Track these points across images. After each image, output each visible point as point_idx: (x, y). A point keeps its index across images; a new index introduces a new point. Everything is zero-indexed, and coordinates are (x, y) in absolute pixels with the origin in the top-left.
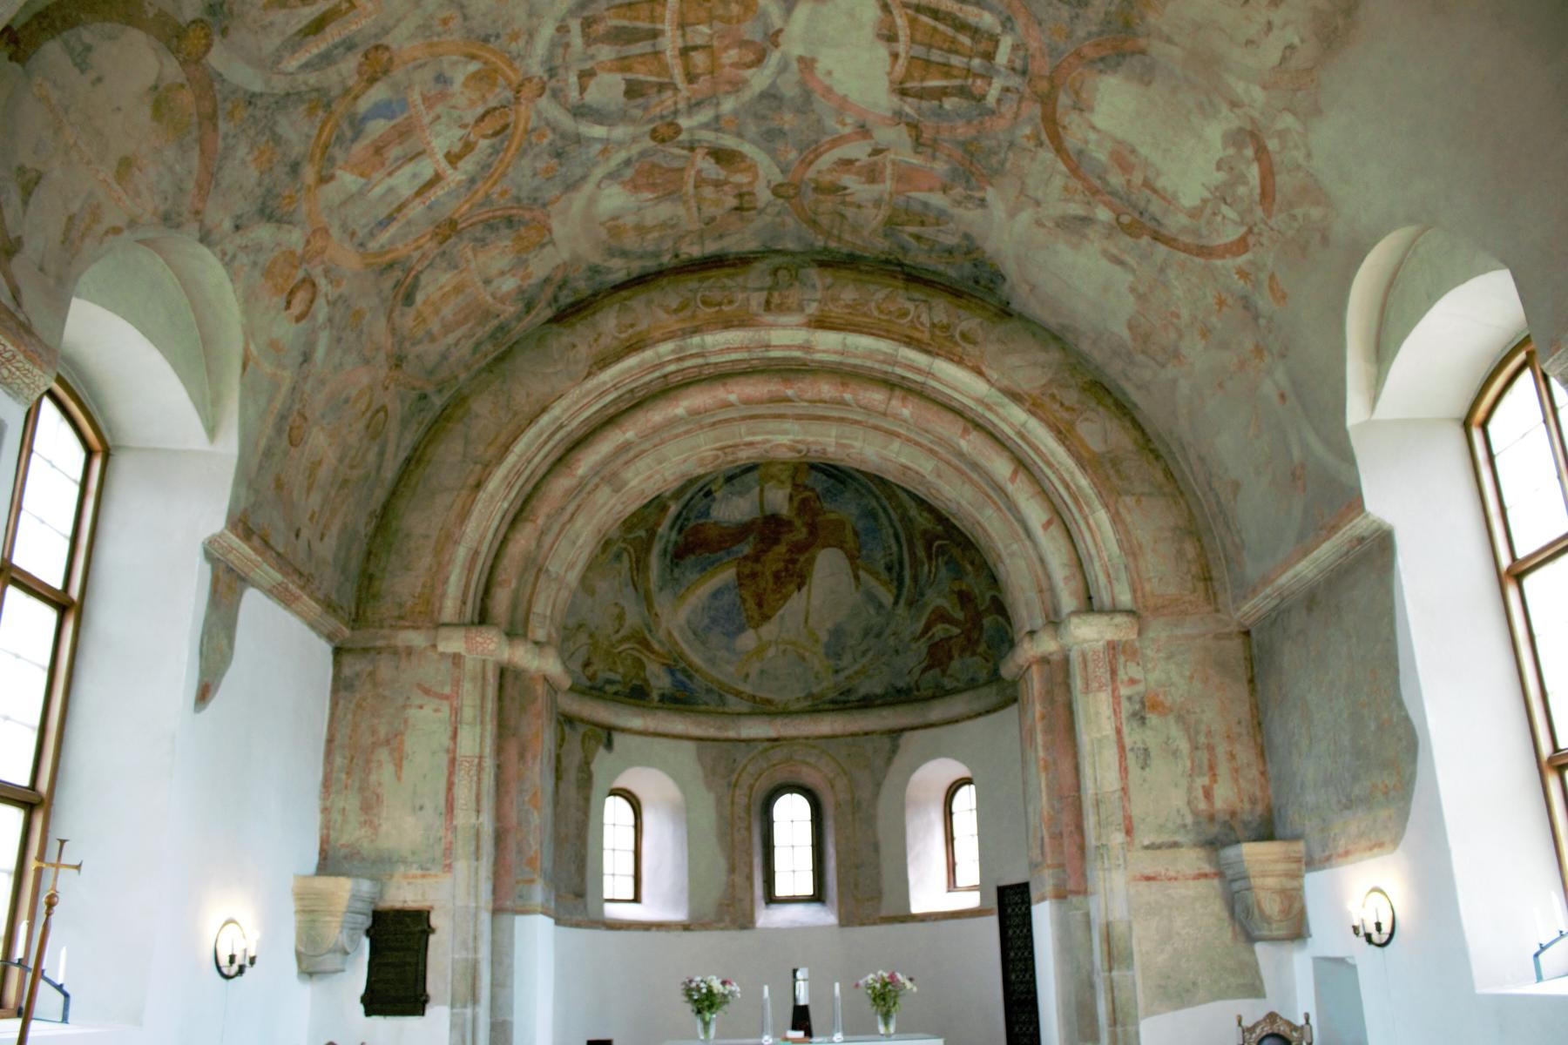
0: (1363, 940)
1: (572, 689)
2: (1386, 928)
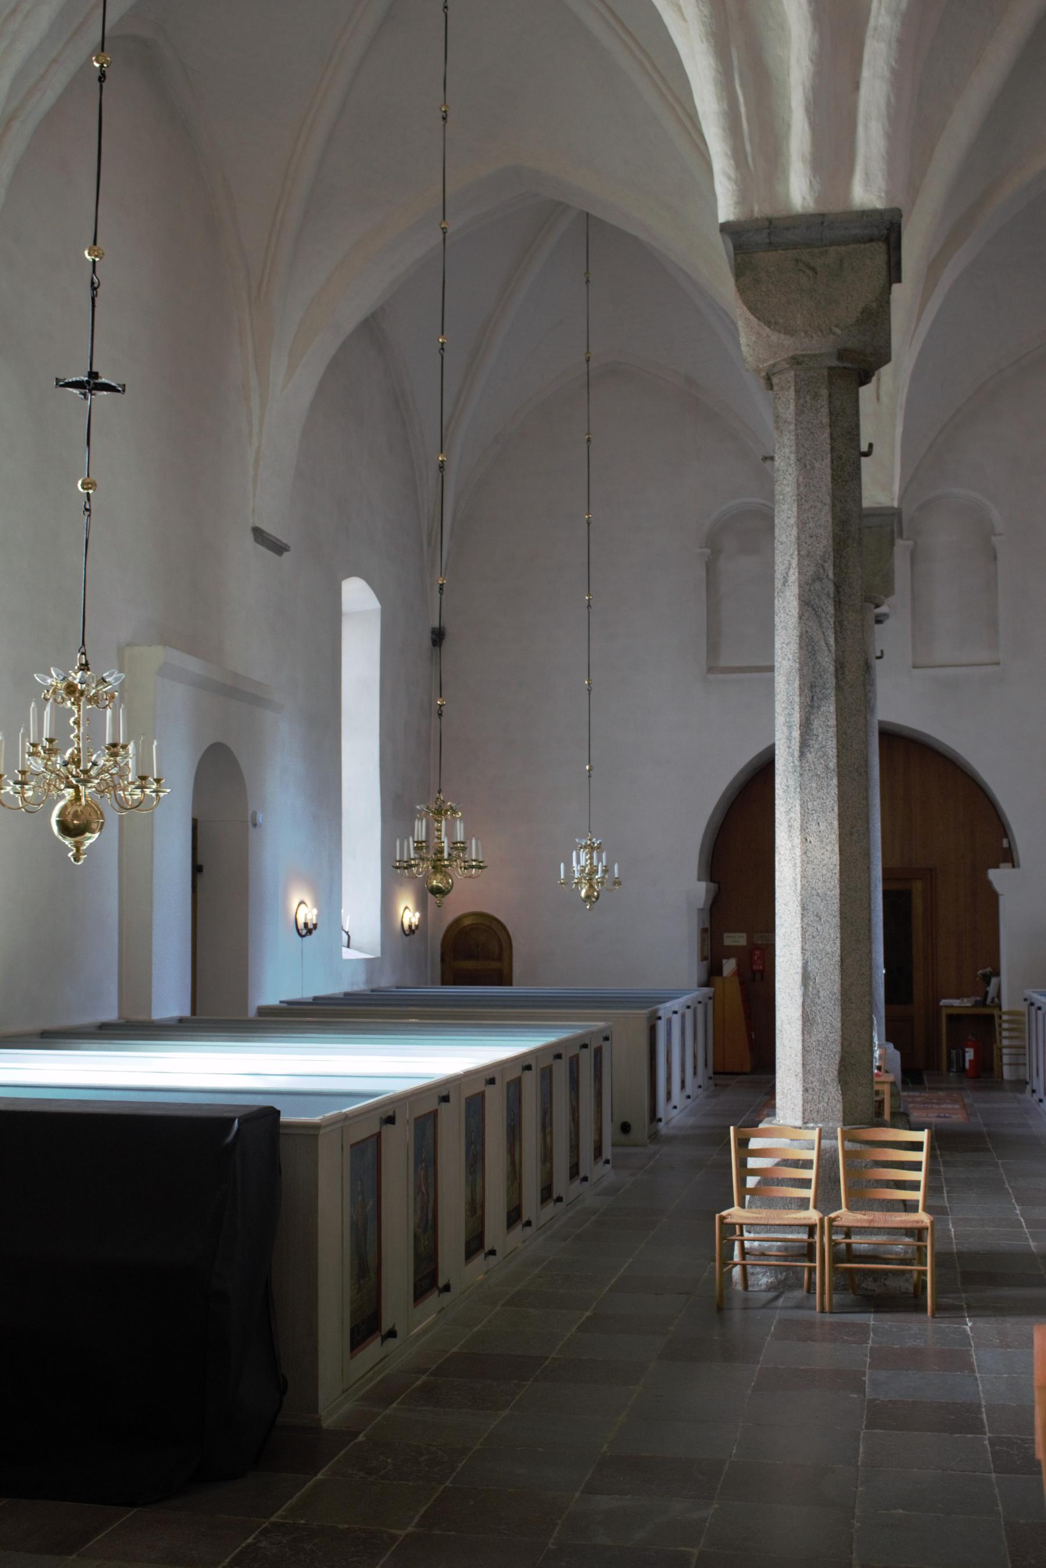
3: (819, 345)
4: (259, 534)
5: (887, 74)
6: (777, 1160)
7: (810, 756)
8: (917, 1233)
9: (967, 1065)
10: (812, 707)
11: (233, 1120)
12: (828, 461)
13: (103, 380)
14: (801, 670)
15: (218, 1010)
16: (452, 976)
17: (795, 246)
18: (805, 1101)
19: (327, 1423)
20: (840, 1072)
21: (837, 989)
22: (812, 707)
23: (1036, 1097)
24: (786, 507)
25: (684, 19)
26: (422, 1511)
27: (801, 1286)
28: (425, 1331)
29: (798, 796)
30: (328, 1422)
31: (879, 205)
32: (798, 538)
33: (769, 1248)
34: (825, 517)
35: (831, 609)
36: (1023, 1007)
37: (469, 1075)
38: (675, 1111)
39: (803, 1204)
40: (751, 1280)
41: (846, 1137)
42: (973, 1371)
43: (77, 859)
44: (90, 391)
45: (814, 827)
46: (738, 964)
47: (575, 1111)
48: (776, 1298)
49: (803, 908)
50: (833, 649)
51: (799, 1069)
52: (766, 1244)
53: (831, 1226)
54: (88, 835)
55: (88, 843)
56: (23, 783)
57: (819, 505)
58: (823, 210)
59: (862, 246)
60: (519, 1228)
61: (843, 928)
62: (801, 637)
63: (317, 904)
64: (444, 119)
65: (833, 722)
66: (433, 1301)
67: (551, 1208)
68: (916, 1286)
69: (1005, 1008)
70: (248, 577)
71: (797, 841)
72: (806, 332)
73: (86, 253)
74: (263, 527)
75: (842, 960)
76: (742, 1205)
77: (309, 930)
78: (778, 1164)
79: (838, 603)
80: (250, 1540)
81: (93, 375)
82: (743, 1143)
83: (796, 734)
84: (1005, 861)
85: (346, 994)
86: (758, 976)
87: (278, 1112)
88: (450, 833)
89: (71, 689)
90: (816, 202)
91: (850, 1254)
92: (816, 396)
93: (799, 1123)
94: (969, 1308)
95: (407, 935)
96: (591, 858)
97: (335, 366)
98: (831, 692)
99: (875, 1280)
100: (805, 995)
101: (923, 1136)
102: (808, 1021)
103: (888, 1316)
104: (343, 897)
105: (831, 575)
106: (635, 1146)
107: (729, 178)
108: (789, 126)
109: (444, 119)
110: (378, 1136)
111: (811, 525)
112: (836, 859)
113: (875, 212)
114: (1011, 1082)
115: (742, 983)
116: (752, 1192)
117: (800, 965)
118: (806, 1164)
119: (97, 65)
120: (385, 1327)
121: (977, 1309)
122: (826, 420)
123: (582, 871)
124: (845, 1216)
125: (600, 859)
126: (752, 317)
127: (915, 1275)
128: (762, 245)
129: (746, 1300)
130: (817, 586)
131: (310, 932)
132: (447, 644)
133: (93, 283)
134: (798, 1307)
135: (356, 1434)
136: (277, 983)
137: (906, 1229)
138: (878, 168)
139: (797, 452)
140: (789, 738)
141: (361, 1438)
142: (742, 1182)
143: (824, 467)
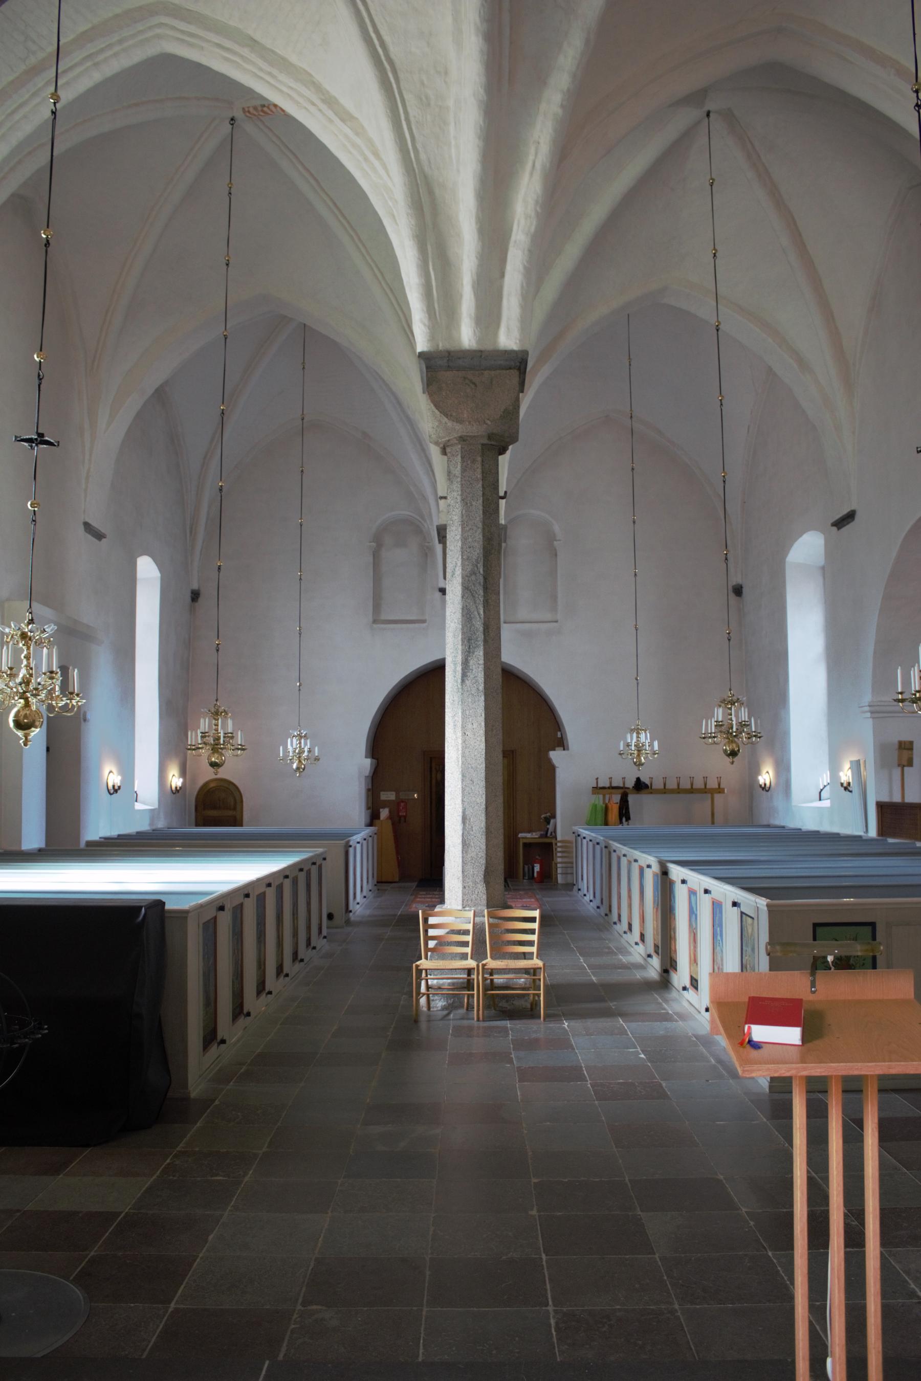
1: (421, 355)
4: (87, 526)
5: (521, 268)
6: (447, 930)
7: (468, 682)
8: (535, 971)
9: (535, 875)
10: (469, 652)
11: (141, 907)
12: (481, 501)
13: (46, 438)
14: (463, 629)
15: (63, 845)
16: (202, 820)
18: (464, 894)
19: (193, 1095)
20: (485, 876)
21: (483, 825)
22: (469, 652)
23: (581, 893)
24: (454, 528)
25: (397, 224)
26: (268, 1140)
27: (463, 1007)
29: (460, 707)
32: (462, 548)
33: (443, 984)
34: (479, 536)
35: (481, 592)
36: (572, 838)
37: (259, 880)
38: (358, 906)
39: (464, 956)
41: (490, 916)
42: (573, 1049)
43: (25, 745)
44: (37, 445)
45: (470, 726)
46: (390, 812)
47: (309, 904)
48: (448, 1014)
49: (463, 776)
50: (482, 616)
51: (460, 874)
52: (441, 981)
53: (483, 968)
54: (33, 729)
55: (32, 734)
57: (475, 528)
59: (504, 372)
60: (282, 978)
61: (487, 788)
62: (463, 609)
64: (227, 265)
65: (482, 662)
66: (242, 1021)
67: (298, 966)
68: (532, 1005)
69: (559, 838)
70: (78, 545)
71: (459, 734)
72: (470, 422)
73: (35, 356)
74: (90, 522)
75: (487, 808)
76: (426, 958)
77: (116, 790)
78: (448, 933)
79: (485, 589)
80: (168, 1161)
81: (41, 435)
82: (426, 920)
83: (459, 668)
84: (559, 746)
85: (137, 833)
86: (403, 819)
87: (164, 903)
88: (224, 725)
89: (24, 636)
91: (492, 986)
92: (474, 461)
93: (460, 907)
94: (564, 1015)
95: (111, 794)
96: (300, 743)
97: (139, 416)
98: (481, 643)
99: (507, 1001)
100: (464, 829)
101: (536, 914)
102: (465, 844)
103: (517, 1022)
104: (137, 773)
105: (482, 571)
106: (336, 928)
107: (425, 325)
108: (461, 296)
109: (227, 265)
110: (215, 918)
111: (470, 540)
112: (483, 746)
113: (513, 351)
114: (562, 885)
115: (393, 824)
116: (432, 950)
117: (461, 810)
118: (466, 932)
119: (44, 236)
121: (572, 1015)
122: (479, 476)
123: (294, 752)
124: (491, 963)
125: (306, 744)
126: (436, 411)
127: (531, 998)
128: (445, 370)
129: (429, 1016)
130: (473, 578)
131: (116, 791)
132: (201, 600)
133: (39, 375)
134: (462, 1019)
135: (214, 1100)
136: (99, 824)
137: (525, 969)
138: (515, 325)
139: (462, 495)
140: (455, 671)
141: (217, 1102)
142: (426, 944)
143: (478, 504)
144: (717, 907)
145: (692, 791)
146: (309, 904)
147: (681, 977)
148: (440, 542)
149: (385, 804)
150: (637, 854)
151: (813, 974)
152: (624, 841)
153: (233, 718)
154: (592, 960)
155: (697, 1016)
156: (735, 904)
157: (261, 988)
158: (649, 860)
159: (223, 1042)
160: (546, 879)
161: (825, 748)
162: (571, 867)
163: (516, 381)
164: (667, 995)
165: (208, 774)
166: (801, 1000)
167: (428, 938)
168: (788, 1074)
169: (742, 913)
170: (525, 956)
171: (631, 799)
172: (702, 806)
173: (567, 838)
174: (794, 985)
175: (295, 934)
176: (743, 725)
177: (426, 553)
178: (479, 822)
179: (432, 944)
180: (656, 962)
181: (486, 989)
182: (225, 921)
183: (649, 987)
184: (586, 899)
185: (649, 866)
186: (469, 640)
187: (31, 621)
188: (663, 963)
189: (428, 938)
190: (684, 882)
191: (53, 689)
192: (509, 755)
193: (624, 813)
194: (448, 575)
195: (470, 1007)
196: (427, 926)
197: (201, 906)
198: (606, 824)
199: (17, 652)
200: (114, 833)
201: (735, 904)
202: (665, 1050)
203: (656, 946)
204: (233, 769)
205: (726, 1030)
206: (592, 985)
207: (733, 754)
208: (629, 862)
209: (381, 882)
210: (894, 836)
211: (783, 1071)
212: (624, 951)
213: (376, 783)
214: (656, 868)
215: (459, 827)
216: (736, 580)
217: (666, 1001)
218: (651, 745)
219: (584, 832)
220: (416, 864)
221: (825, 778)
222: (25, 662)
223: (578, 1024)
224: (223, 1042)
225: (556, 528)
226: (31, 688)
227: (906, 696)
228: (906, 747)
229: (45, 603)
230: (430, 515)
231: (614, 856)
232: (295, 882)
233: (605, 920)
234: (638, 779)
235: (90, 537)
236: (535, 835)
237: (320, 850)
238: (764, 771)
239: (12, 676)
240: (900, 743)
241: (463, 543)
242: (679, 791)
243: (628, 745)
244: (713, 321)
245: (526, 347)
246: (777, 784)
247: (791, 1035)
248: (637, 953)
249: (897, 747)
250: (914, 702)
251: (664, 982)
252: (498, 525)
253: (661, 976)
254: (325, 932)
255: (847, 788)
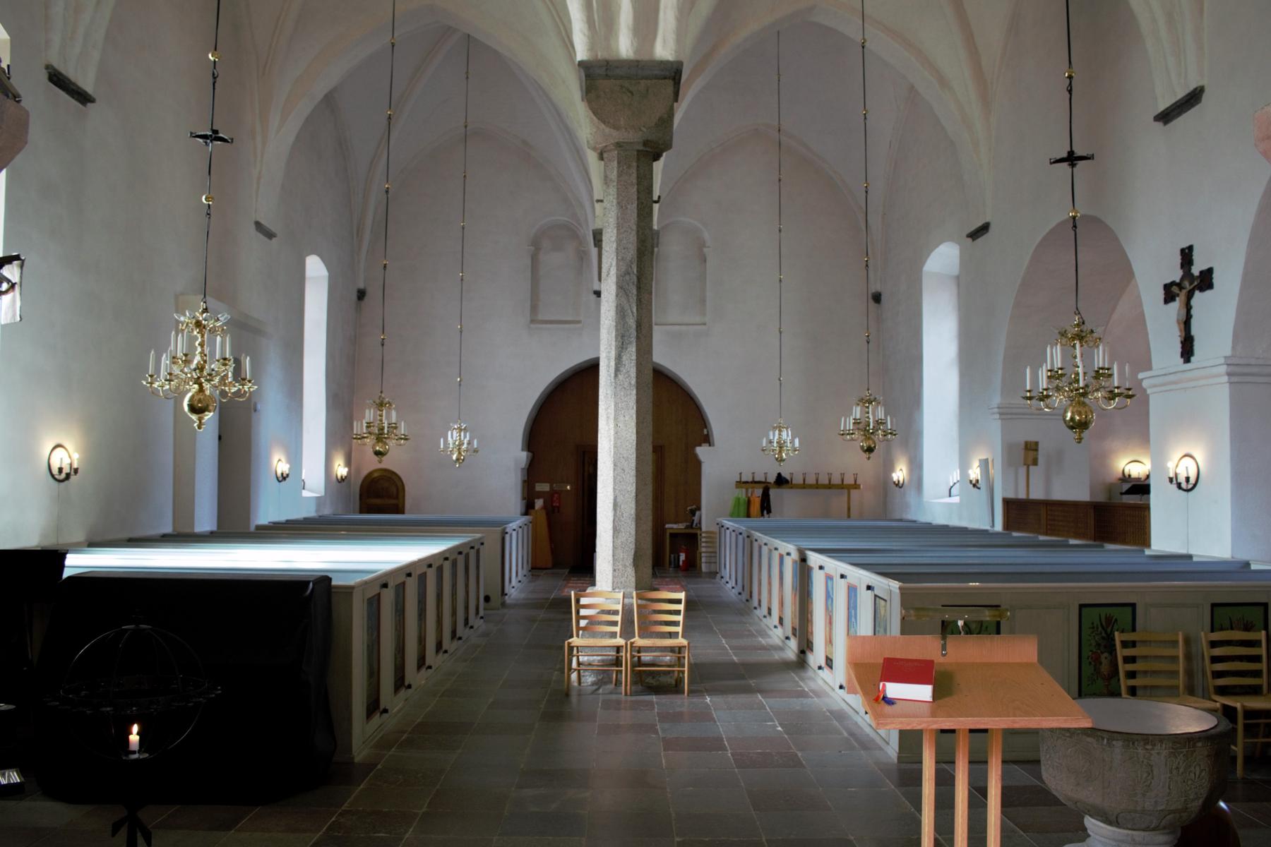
0: (1174, 486)
1: (581, 63)
2: (1192, 480)
3: (633, 137)
4: (259, 226)
7: (621, 377)
8: (680, 649)
12: (635, 205)
15: (234, 528)
16: (366, 508)
17: (622, 78)
18: (614, 577)
19: (357, 760)
21: (633, 511)
28: (399, 711)
30: (358, 758)
31: (670, 58)
34: (633, 237)
35: (635, 291)
36: (715, 529)
37: (420, 561)
39: (613, 635)
40: (583, 680)
41: (639, 597)
43: (199, 427)
47: (467, 586)
51: (611, 558)
52: (591, 658)
56: (170, 380)
58: (639, 58)
63: (289, 461)
65: (634, 357)
66: (403, 693)
67: (456, 643)
69: (704, 529)
70: (252, 251)
71: (612, 426)
77: (284, 478)
79: (639, 288)
81: (215, 132)
82: (578, 601)
83: (613, 363)
88: (389, 416)
89: (198, 324)
90: (635, 53)
92: (629, 166)
97: (308, 121)
98: (634, 340)
101: (682, 596)
102: (616, 530)
104: (304, 460)
108: (620, 7)
110: (379, 595)
112: (634, 437)
113: (668, 62)
115: (547, 514)
116: (584, 629)
118: (615, 613)
120: (382, 707)
121: (711, 692)
124: (639, 641)
128: (601, 78)
130: (627, 277)
132: (366, 299)
134: (611, 693)
136: (267, 511)
140: (608, 366)
142: (578, 623)
143: (633, 208)
144: (852, 590)
145: (830, 486)
146: (467, 586)
147: (816, 657)
148: (595, 245)
149: (540, 495)
150: (777, 542)
151: (944, 638)
152: (765, 531)
153: (397, 409)
154: (735, 642)
155: (832, 694)
156: (869, 588)
157: (421, 662)
158: (789, 548)
159: (385, 711)
160: (691, 568)
161: (956, 447)
162: (715, 556)
163: (670, 89)
164: (803, 674)
165: (371, 464)
166: (932, 662)
167: (579, 618)
168: (919, 727)
169: (876, 596)
170: (672, 635)
171: (773, 492)
172: (839, 501)
173: (711, 529)
174: (926, 647)
175: (454, 613)
176: (879, 423)
177: (582, 256)
178: (629, 508)
179: (583, 623)
180: (793, 644)
181: (633, 666)
182: (388, 597)
183: (787, 666)
184: (729, 587)
185: (788, 554)
186: (623, 336)
187: (205, 310)
188: (800, 644)
189: (579, 618)
190: (821, 568)
191: (226, 375)
192: (658, 450)
193: (766, 507)
194: (604, 275)
195: (618, 683)
196: (579, 606)
197: (366, 583)
198: (748, 516)
199: (192, 340)
200: (283, 518)
201: (869, 588)
202: (805, 724)
203: (794, 629)
204: (397, 459)
205: (862, 688)
206: (734, 664)
207: (870, 450)
208: (770, 550)
209: (535, 568)
210: (1019, 530)
211: (914, 724)
212: (763, 634)
213: (532, 474)
214: (795, 555)
215: (610, 514)
216: (875, 287)
217: (802, 679)
218: (792, 442)
219: (728, 523)
220: (568, 550)
221: (955, 476)
222: (199, 349)
223: (719, 699)
224: (385, 711)
225: (706, 235)
226: (205, 373)
227: (1033, 394)
228: (1031, 448)
229: (219, 298)
230: (586, 220)
231: (756, 545)
232: (454, 564)
233: (746, 605)
234: (779, 475)
235: (261, 236)
236: (681, 526)
237: (478, 535)
238: (898, 469)
239: (187, 362)
240: (1026, 443)
241: (618, 245)
242: (817, 486)
243: (771, 442)
244: (859, 39)
245: (682, 58)
246: (911, 480)
247: (923, 692)
248: (776, 635)
249: (1023, 446)
250: (1041, 400)
251: (801, 663)
252: (651, 228)
253: (798, 656)
254: (482, 613)
255: (975, 485)
